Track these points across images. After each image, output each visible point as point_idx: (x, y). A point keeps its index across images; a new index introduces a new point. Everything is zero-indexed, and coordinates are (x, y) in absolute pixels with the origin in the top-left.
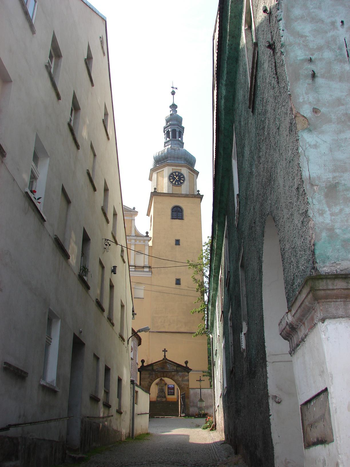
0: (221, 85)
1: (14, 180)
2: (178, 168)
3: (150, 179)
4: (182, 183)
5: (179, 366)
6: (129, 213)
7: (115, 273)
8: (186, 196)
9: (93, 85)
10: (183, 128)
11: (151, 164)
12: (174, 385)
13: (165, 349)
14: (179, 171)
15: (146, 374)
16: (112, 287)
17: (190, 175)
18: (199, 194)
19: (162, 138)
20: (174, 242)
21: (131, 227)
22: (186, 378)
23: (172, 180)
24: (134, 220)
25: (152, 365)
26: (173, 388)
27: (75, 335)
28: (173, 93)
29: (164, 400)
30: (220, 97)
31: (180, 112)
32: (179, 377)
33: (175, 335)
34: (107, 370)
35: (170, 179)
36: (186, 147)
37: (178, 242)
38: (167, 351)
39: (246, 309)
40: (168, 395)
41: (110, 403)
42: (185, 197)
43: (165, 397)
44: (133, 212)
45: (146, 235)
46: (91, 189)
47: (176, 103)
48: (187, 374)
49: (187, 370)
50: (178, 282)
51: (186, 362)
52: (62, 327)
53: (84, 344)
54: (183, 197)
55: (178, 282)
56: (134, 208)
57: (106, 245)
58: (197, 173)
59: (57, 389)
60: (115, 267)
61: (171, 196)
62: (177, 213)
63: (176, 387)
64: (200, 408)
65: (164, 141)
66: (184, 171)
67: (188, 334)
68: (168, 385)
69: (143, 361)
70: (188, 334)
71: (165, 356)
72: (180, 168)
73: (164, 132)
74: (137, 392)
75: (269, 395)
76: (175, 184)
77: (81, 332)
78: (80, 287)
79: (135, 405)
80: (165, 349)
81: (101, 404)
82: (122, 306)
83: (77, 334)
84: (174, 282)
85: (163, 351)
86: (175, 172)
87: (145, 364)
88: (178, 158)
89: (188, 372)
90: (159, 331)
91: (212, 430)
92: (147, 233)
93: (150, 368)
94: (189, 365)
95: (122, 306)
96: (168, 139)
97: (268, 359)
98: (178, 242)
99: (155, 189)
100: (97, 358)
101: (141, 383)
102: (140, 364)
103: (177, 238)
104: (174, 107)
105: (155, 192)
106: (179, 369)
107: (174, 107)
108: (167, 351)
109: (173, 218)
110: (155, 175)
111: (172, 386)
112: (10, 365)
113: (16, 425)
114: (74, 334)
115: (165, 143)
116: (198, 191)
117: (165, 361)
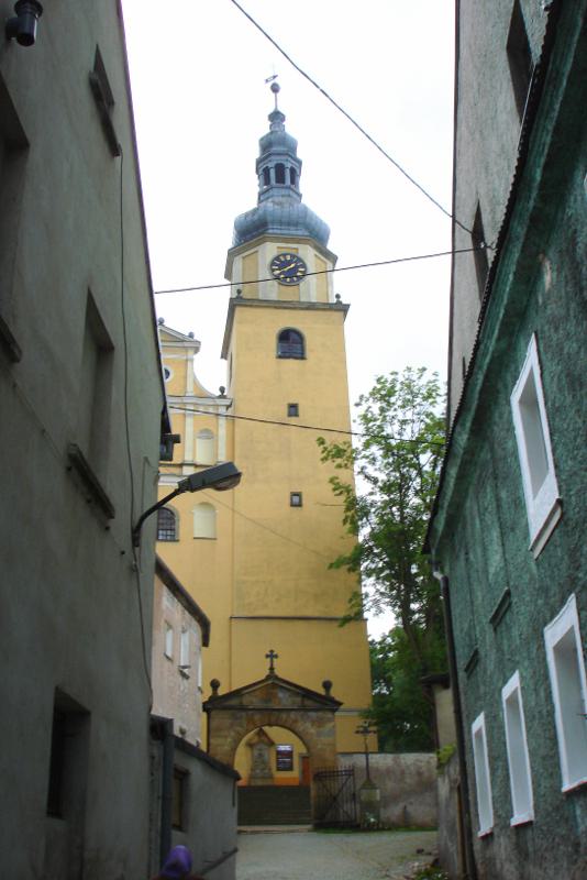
5: (307, 694)
6: (180, 344)
8: (311, 307)
10: (300, 163)
11: (228, 239)
14: (294, 252)
15: (222, 719)
17: (319, 261)
18: (339, 303)
19: (253, 184)
21: (185, 378)
22: (329, 726)
24: (192, 360)
28: (275, 89)
29: (269, 782)
31: (291, 128)
32: (308, 725)
36: (304, 201)
37: (293, 409)
38: (276, 656)
39: (160, 824)
40: (278, 769)
43: (271, 777)
44: (189, 344)
45: (219, 393)
47: (280, 109)
48: (329, 715)
51: (327, 685)
54: (302, 309)
56: (191, 335)
58: (333, 258)
61: (276, 308)
62: (291, 344)
64: (371, 806)
65: (258, 189)
66: (308, 254)
67: (323, 623)
69: (215, 685)
71: (272, 669)
72: (295, 246)
73: (257, 171)
79: (176, 834)
80: (272, 651)
85: (267, 656)
87: (222, 691)
88: (289, 224)
92: (222, 390)
93: (234, 702)
94: (335, 693)
98: (293, 409)
101: (212, 741)
102: (209, 692)
103: (293, 401)
104: (276, 117)
106: (309, 703)
107: (276, 117)
108: (276, 656)
111: (287, 748)
115: (260, 194)
116: (338, 296)
117: (273, 682)
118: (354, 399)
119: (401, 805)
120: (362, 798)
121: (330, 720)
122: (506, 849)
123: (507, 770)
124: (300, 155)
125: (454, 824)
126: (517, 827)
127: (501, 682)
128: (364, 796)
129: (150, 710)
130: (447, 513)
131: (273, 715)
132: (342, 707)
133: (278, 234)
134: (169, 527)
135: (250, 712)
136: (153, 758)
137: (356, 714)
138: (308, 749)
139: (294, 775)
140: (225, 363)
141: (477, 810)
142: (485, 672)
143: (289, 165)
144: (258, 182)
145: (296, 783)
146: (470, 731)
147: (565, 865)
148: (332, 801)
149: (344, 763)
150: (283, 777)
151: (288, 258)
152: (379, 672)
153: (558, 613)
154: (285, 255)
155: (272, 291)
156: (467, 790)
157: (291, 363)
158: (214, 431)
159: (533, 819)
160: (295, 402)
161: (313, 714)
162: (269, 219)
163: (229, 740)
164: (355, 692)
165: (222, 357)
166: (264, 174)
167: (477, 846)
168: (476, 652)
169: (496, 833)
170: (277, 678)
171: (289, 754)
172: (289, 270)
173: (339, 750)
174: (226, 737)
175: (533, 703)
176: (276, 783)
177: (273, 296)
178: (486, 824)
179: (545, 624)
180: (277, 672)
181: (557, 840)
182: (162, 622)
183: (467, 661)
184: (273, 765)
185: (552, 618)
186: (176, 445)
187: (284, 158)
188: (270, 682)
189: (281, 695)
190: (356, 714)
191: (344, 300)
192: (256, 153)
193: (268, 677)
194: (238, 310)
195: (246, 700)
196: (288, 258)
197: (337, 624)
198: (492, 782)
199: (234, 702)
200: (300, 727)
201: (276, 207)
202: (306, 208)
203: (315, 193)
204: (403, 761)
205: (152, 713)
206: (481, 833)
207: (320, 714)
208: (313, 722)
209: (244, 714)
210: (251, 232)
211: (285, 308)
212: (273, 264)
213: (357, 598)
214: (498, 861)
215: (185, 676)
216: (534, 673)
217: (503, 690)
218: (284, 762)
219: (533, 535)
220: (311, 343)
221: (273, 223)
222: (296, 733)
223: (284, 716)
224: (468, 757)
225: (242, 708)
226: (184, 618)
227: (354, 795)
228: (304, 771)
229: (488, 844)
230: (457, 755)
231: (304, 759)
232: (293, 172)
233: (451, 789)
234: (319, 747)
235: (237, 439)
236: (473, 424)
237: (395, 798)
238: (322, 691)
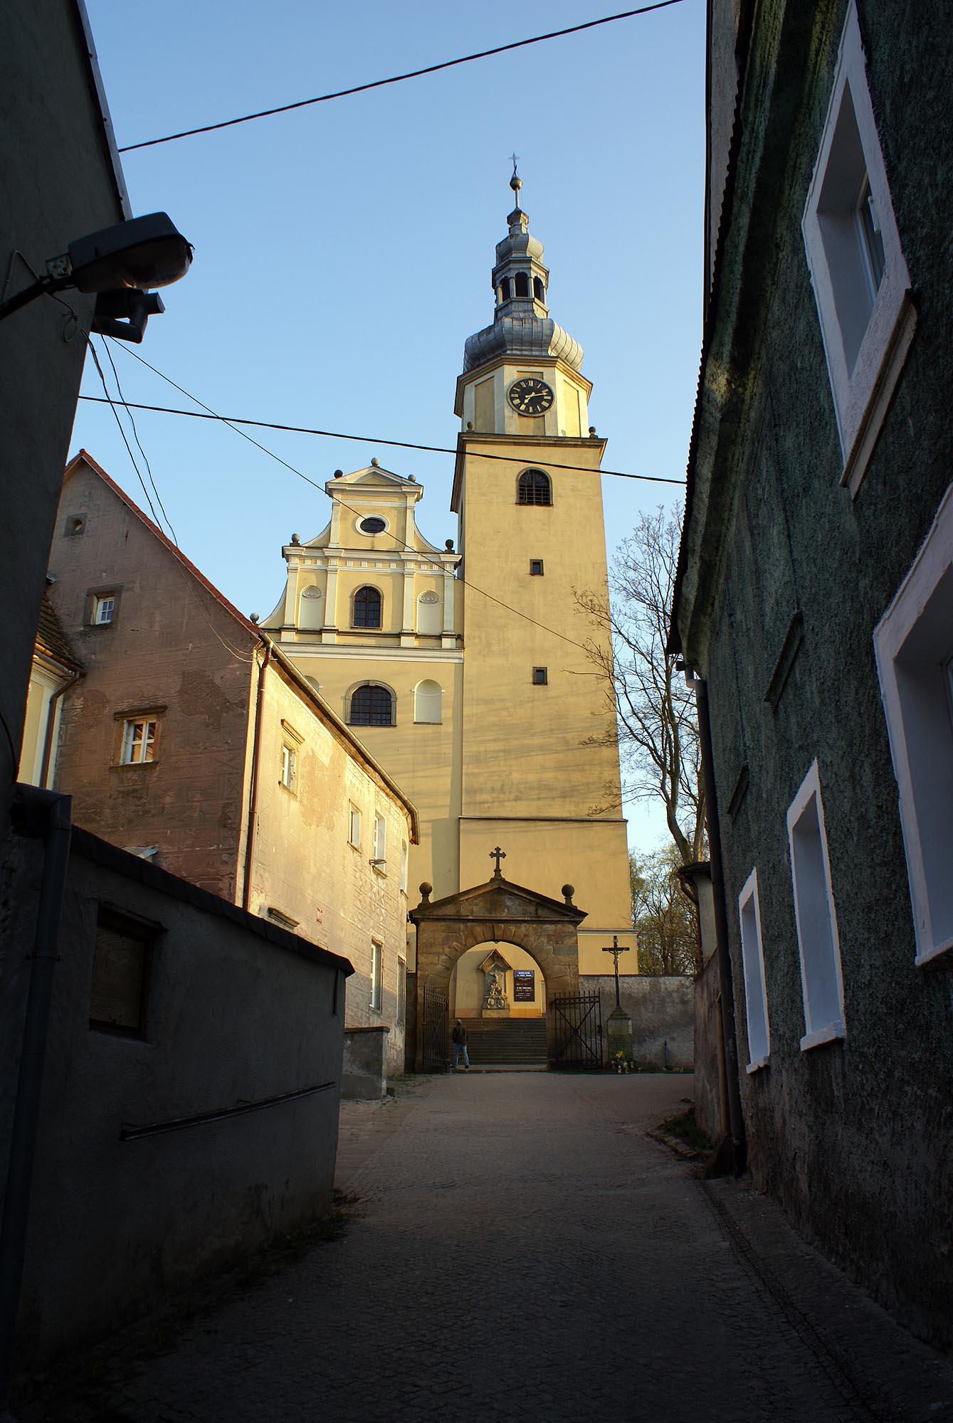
3: (459, 410)
5: (543, 902)
12: (532, 972)
13: (498, 849)
20: (527, 568)
22: (569, 941)
23: (517, 401)
26: (531, 982)
28: (514, 185)
29: (502, 1014)
33: (532, 824)
37: (537, 567)
38: (504, 855)
40: (517, 999)
42: (554, 445)
48: (570, 928)
50: (540, 676)
51: (567, 891)
54: (549, 445)
55: (540, 676)
56: (410, 478)
61: (515, 444)
63: (539, 977)
64: (618, 1041)
68: (516, 972)
69: (425, 890)
71: (498, 870)
76: (527, 410)
80: (498, 849)
85: (492, 855)
87: (432, 898)
90: (484, 816)
91: (646, 527)
92: (449, 544)
93: (449, 910)
98: (537, 567)
101: (421, 959)
104: (515, 217)
107: (515, 217)
108: (504, 855)
110: (470, 391)
115: (497, 311)
119: (661, 1040)
122: (790, 1094)
123: (795, 953)
125: (715, 1056)
126: (810, 1052)
127: (786, 797)
129: (15, 776)
130: (701, 558)
131: (494, 928)
132: (585, 923)
134: (384, 710)
139: (537, 1007)
140: (455, 516)
141: (745, 1032)
142: (759, 797)
143: (533, 275)
146: (736, 908)
147: (919, 1126)
150: (519, 1009)
151: (531, 383)
153: (908, 568)
154: (526, 381)
155: (514, 424)
156: (730, 1003)
157: (536, 511)
158: (440, 595)
159: (843, 1034)
162: (507, 337)
163: (444, 957)
166: (499, 281)
167: (745, 1089)
168: (746, 769)
169: (773, 1068)
170: (503, 880)
172: (535, 398)
174: (439, 954)
175: (847, 807)
176: (512, 1015)
178: (758, 1053)
179: (875, 621)
181: (897, 1074)
182: (345, 803)
183: (730, 796)
184: (510, 993)
185: (890, 597)
189: (509, 903)
191: (600, 434)
192: (493, 263)
194: (473, 467)
195: (464, 910)
196: (531, 383)
198: (769, 978)
199: (449, 910)
201: (515, 323)
203: (562, 312)
206: (750, 1069)
209: (462, 926)
210: (484, 354)
212: (512, 391)
213: (613, 790)
214: (777, 1115)
215: (379, 874)
216: (851, 744)
217: (789, 813)
218: (524, 991)
219: (847, 446)
221: (512, 342)
223: (513, 928)
224: (732, 951)
226: (378, 801)
227: (600, 1027)
229: (761, 1085)
230: (718, 959)
233: (711, 1006)
236: (735, 343)
237: (653, 1033)
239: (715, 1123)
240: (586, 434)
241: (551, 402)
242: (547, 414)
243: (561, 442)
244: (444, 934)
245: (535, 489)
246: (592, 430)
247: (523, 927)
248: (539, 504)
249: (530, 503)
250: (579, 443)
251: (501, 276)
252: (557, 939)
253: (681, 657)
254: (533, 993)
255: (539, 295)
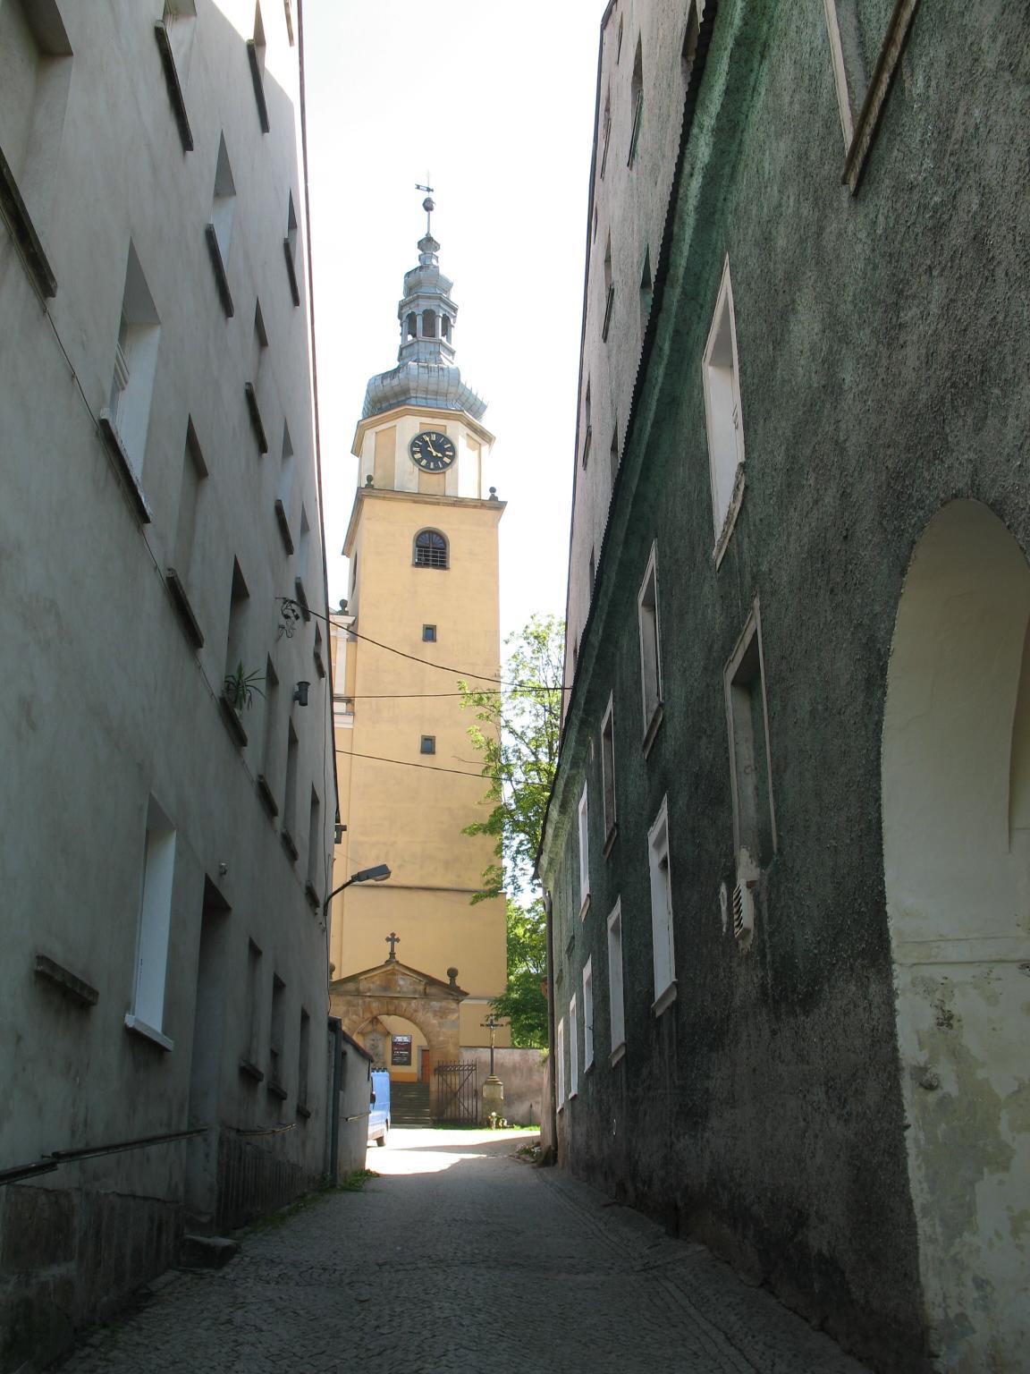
0: (695, 131)
1: (73, 376)
2: (437, 421)
3: (357, 450)
4: (446, 465)
5: (431, 981)
7: (304, 704)
9: (265, 127)
13: (393, 935)
16: (293, 741)
18: (493, 498)
20: (420, 633)
22: (453, 1017)
23: (418, 456)
25: (354, 978)
26: (408, 1046)
27: (208, 882)
28: (428, 206)
30: (687, 168)
31: (446, 264)
32: (430, 1015)
34: (279, 986)
35: (413, 453)
37: (430, 633)
38: (398, 940)
40: (394, 1063)
41: (283, 1087)
46: (252, 446)
48: (453, 1005)
49: (452, 990)
50: (428, 746)
51: (452, 973)
52: (179, 854)
53: (228, 909)
55: (428, 746)
57: (287, 617)
59: (168, 1043)
60: (304, 686)
61: (415, 502)
62: (431, 551)
65: (398, 341)
66: (459, 435)
70: (452, 894)
71: (392, 954)
73: (400, 317)
74: (344, 1054)
75: (904, 1064)
76: (427, 467)
77: (223, 873)
78: (217, 736)
80: (393, 935)
81: (262, 1085)
82: (315, 802)
83: (213, 878)
84: (418, 745)
85: (388, 940)
86: (428, 434)
89: (458, 1001)
93: (351, 986)
94: (460, 982)
95: (315, 802)
96: (410, 338)
97: (896, 952)
98: (430, 633)
99: (370, 478)
100: (255, 952)
103: (429, 622)
104: (427, 244)
105: (369, 486)
106: (432, 990)
107: (427, 244)
108: (398, 940)
109: (417, 565)
110: (370, 437)
111: (406, 1039)
112: (53, 966)
113: (71, 1155)
114: (207, 878)
116: (493, 490)
118: (504, 635)
120: (484, 1095)
121: (454, 1011)
124: (454, 297)
128: (486, 1092)
133: (420, 399)
135: (368, 1000)
136: (329, 1042)
137: (485, 1002)
138: (429, 1041)
144: (399, 329)
145: (415, 1079)
148: (452, 1096)
149: (468, 1057)
152: (516, 950)
157: (430, 573)
160: (431, 734)
161: (435, 1004)
162: (412, 385)
164: (487, 978)
165: (343, 554)
166: (409, 321)
171: (408, 1046)
172: (434, 453)
173: (461, 1044)
177: (412, 487)
180: (398, 957)
184: (389, 1057)
186: (343, 832)
187: (437, 302)
188: (389, 968)
190: (485, 1002)
192: (399, 295)
193: (388, 962)
194: (368, 503)
195: (363, 986)
197: (469, 898)
200: (420, 1016)
202: (457, 373)
204: (531, 1058)
205: (330, 1015)
207: (444, 1004)
208: (435, 1013)
211: (426, 503)
212: (413, 444)
220: (455, 552)
222: (415, 1023)
223: (404, 1004)
225: (358, 993)
227: (476, 1091)
228: (424, 1066)
231: (425, 1052)
232: (446, 320)
234: (441, 1038)
235: (360, 667)
238: (447, 980)
239: (297, 702)
240: (486, 496)
241: (452, 458)
242: (449, 472)
243: (459, 503)
244: (344, 1008)
245: (431, 551)
246: (493, 490)
247: (414, 1003)
248: (435, 566)
249: (426, 565)
250: (479, 504)
251: (407, 311)
252: (442, 1014)
253: (540, 881)
254: (409, 1057)
255: (446, 332)
